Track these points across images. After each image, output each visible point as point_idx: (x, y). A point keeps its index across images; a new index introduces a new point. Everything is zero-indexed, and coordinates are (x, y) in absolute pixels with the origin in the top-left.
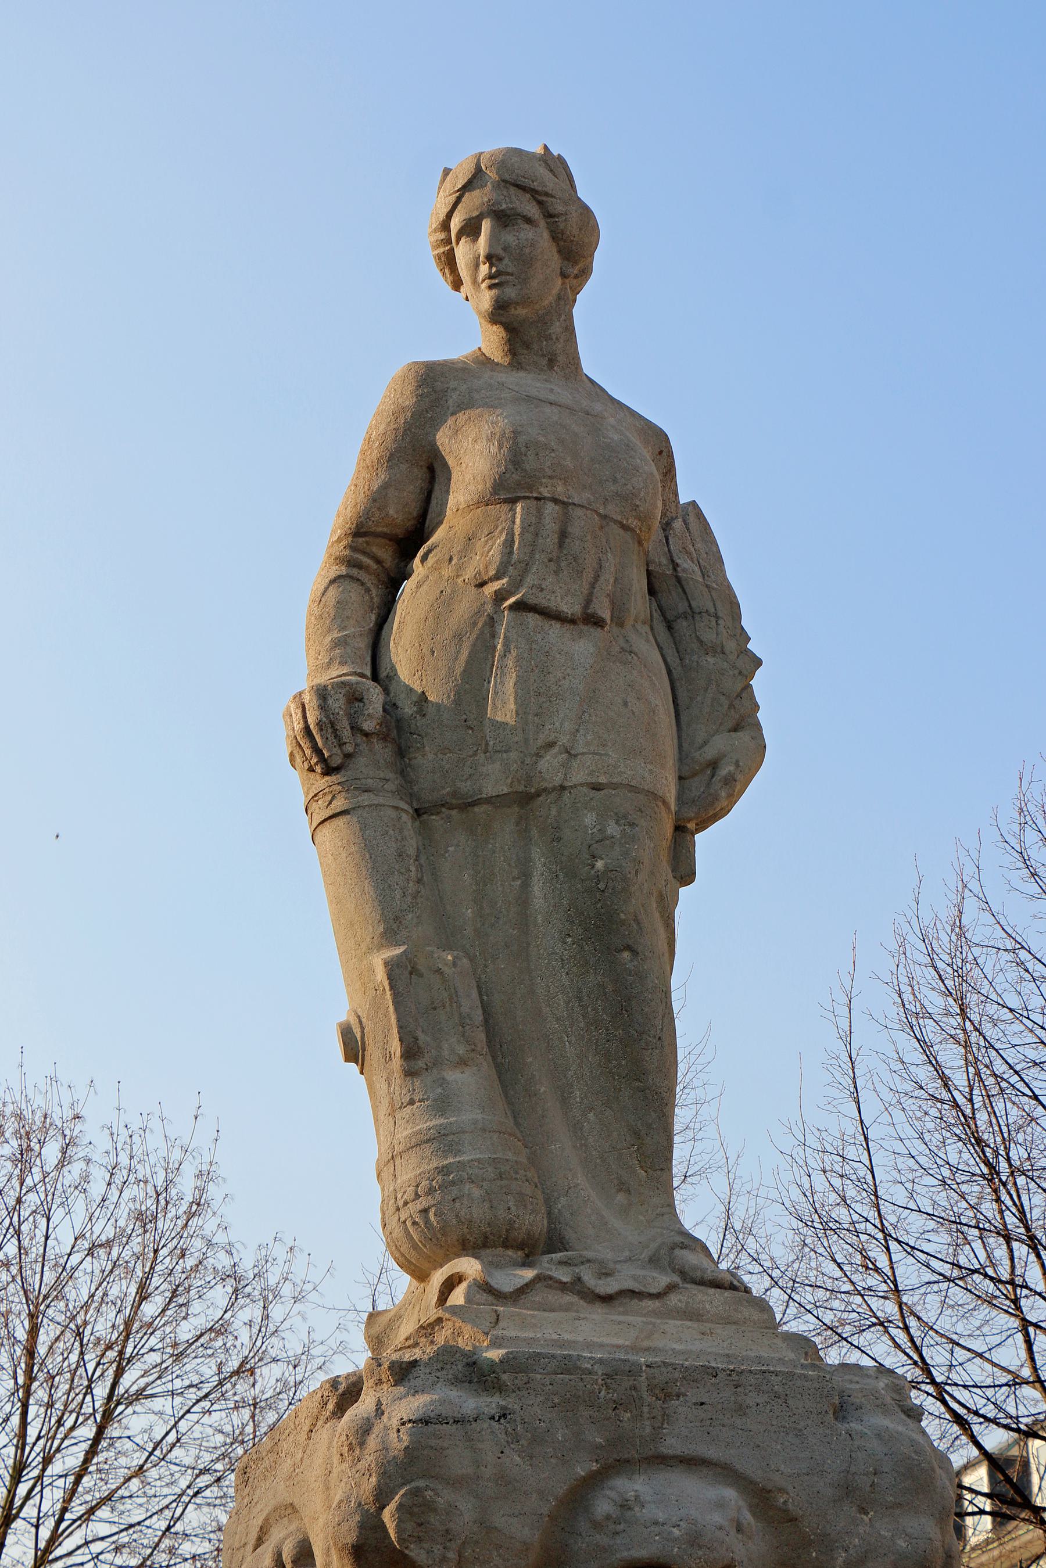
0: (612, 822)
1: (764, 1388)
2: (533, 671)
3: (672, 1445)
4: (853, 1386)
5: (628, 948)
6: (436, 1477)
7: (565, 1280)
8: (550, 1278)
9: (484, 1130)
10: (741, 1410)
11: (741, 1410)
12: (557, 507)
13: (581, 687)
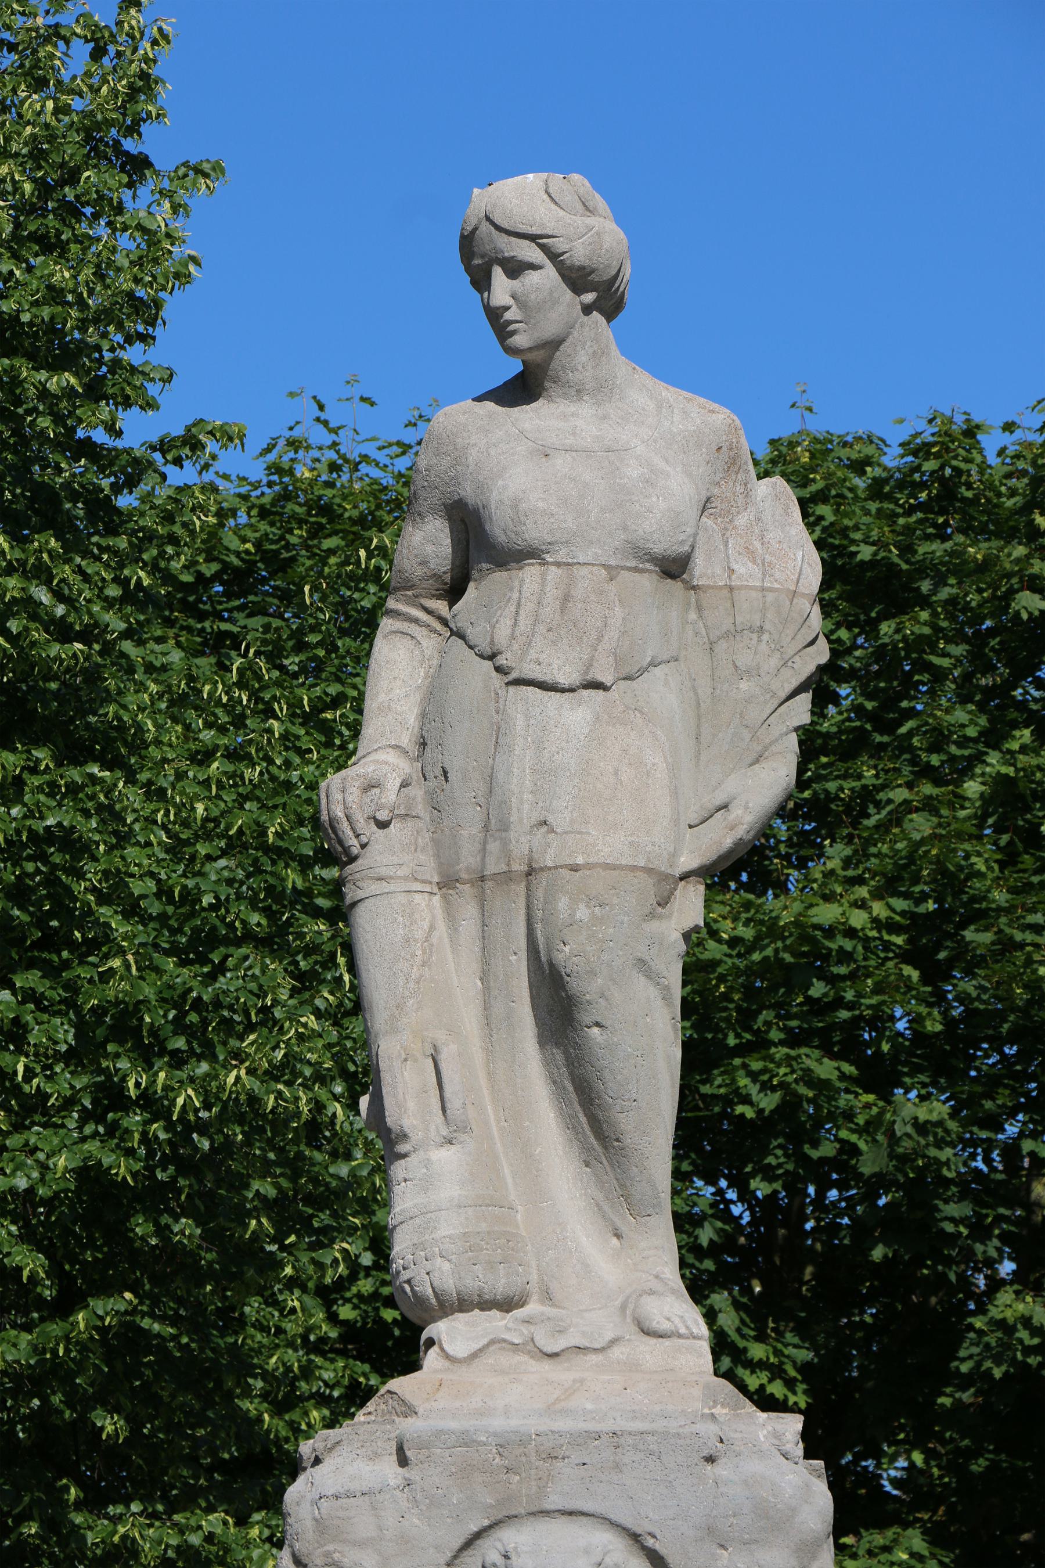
0: (582, 906)
1: (641, 1447)
2: (529, 747)
3: (554, 1501)
4: (738, 1435)
5: (597, 1024)
6: (344, 1541)
7: (516, 1341)
8: (504, 1341)
9: (460, 1207)
10: (618, 1467)
11: (618, 1467)
12: (560, 571)
13: (572, 762)
